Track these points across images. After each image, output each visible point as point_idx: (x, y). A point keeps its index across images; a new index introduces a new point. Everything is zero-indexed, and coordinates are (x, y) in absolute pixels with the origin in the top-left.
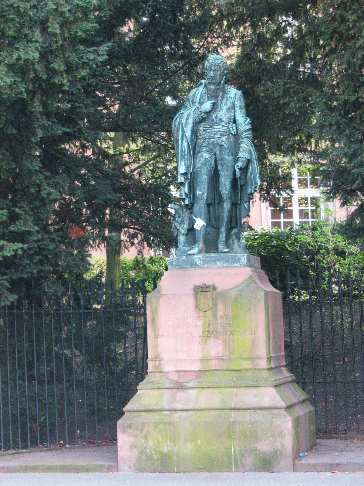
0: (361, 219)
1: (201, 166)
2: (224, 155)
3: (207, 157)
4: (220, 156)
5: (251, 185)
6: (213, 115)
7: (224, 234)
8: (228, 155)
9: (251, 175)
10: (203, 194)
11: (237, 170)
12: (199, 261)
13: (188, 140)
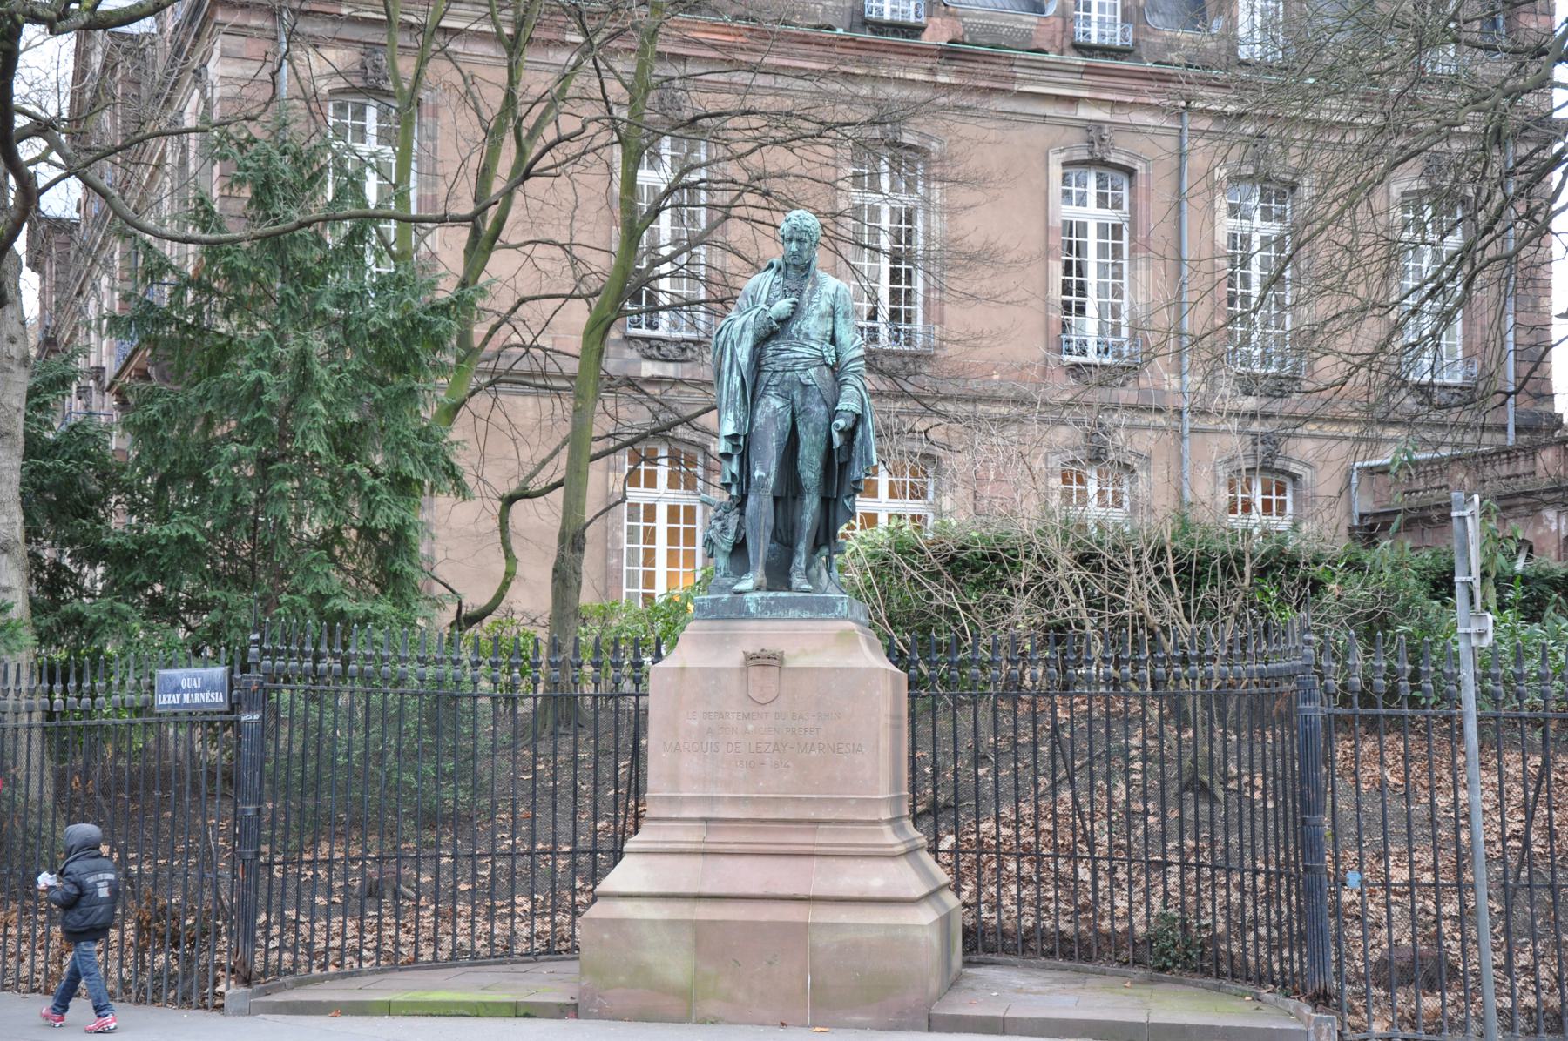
10: (768, 475)
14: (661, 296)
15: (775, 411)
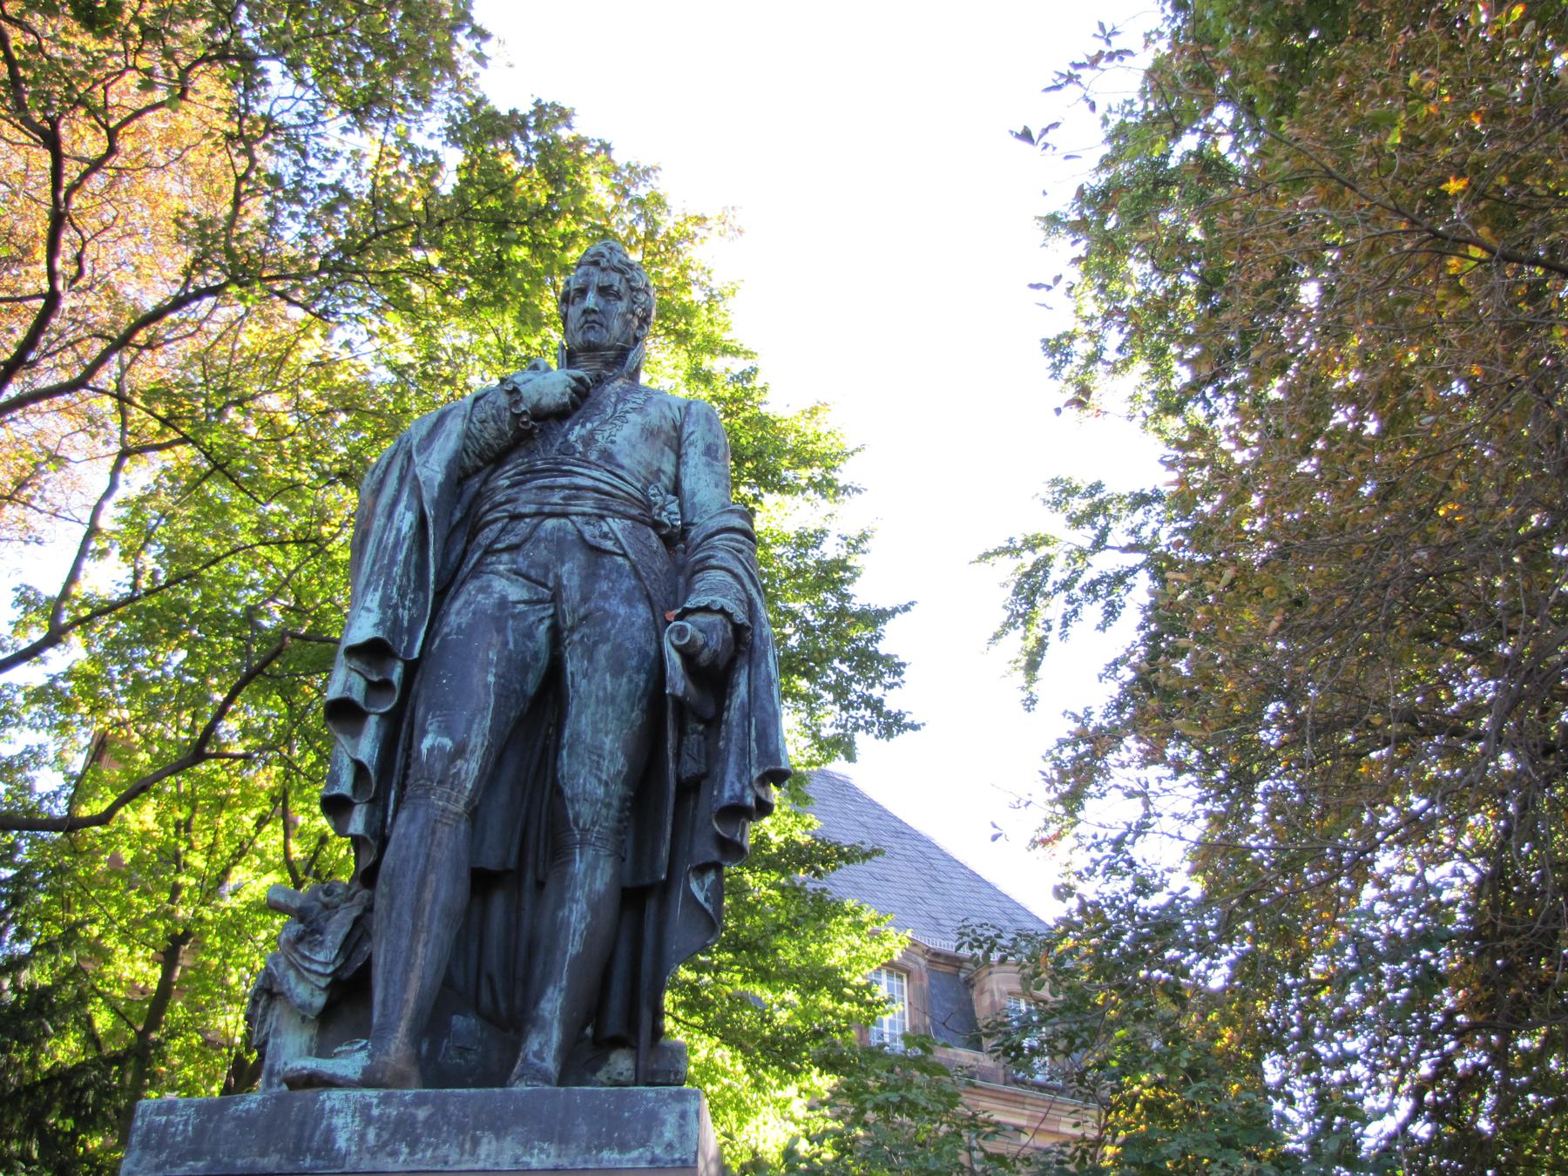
0: (1519, 771)
1: (472, 626)
2: (605, 596)
3: (512, 598)
4: (585, 599)
5: (743, 770)
6: (571, 429)
7: (556, 1036)
8: (628, 600)
9: (747, 715)
10: (460, 751)
11: (674, 660)
12: (357, 1125)
13: (426, 497)
14: (70, 13)
15: (503, 603)
